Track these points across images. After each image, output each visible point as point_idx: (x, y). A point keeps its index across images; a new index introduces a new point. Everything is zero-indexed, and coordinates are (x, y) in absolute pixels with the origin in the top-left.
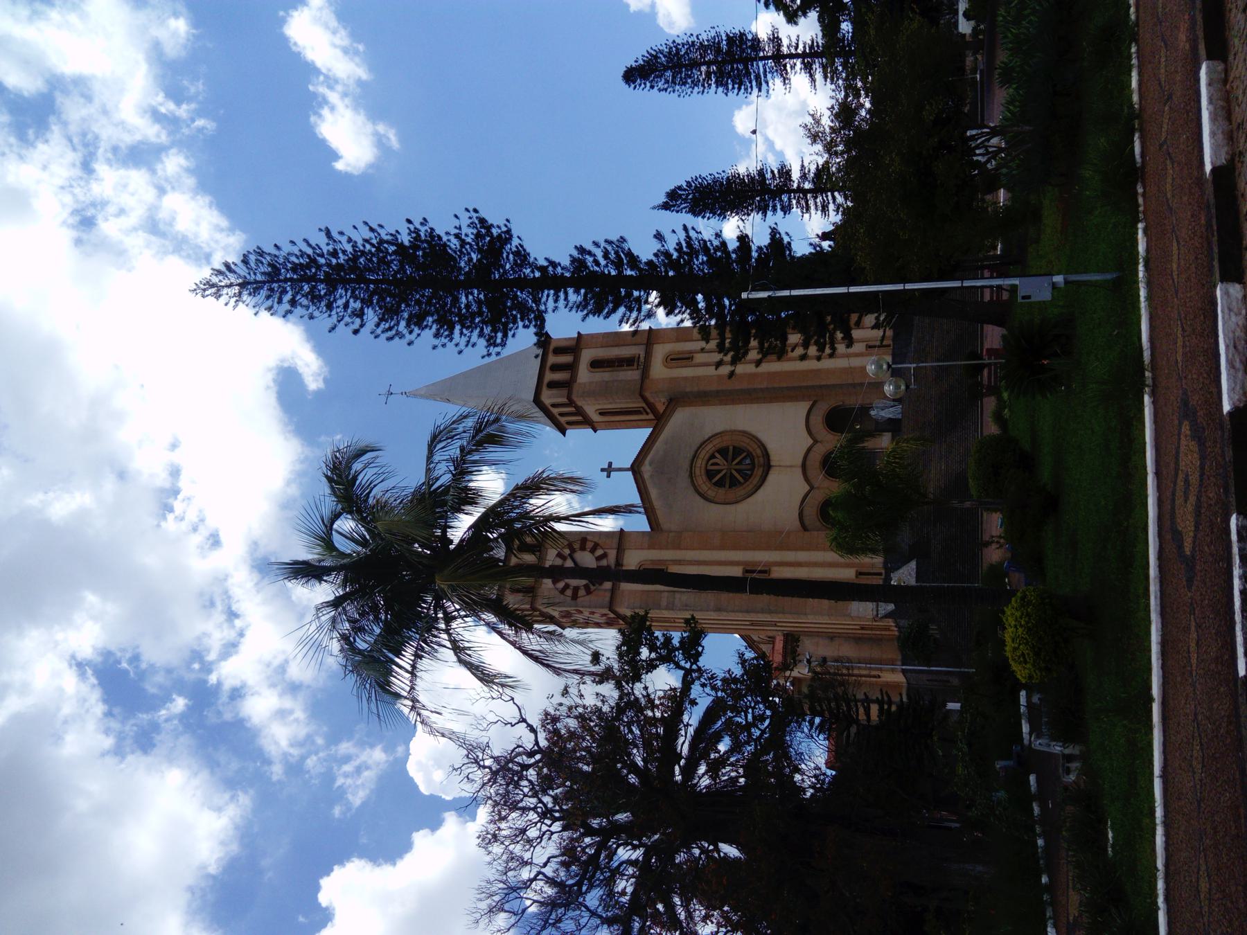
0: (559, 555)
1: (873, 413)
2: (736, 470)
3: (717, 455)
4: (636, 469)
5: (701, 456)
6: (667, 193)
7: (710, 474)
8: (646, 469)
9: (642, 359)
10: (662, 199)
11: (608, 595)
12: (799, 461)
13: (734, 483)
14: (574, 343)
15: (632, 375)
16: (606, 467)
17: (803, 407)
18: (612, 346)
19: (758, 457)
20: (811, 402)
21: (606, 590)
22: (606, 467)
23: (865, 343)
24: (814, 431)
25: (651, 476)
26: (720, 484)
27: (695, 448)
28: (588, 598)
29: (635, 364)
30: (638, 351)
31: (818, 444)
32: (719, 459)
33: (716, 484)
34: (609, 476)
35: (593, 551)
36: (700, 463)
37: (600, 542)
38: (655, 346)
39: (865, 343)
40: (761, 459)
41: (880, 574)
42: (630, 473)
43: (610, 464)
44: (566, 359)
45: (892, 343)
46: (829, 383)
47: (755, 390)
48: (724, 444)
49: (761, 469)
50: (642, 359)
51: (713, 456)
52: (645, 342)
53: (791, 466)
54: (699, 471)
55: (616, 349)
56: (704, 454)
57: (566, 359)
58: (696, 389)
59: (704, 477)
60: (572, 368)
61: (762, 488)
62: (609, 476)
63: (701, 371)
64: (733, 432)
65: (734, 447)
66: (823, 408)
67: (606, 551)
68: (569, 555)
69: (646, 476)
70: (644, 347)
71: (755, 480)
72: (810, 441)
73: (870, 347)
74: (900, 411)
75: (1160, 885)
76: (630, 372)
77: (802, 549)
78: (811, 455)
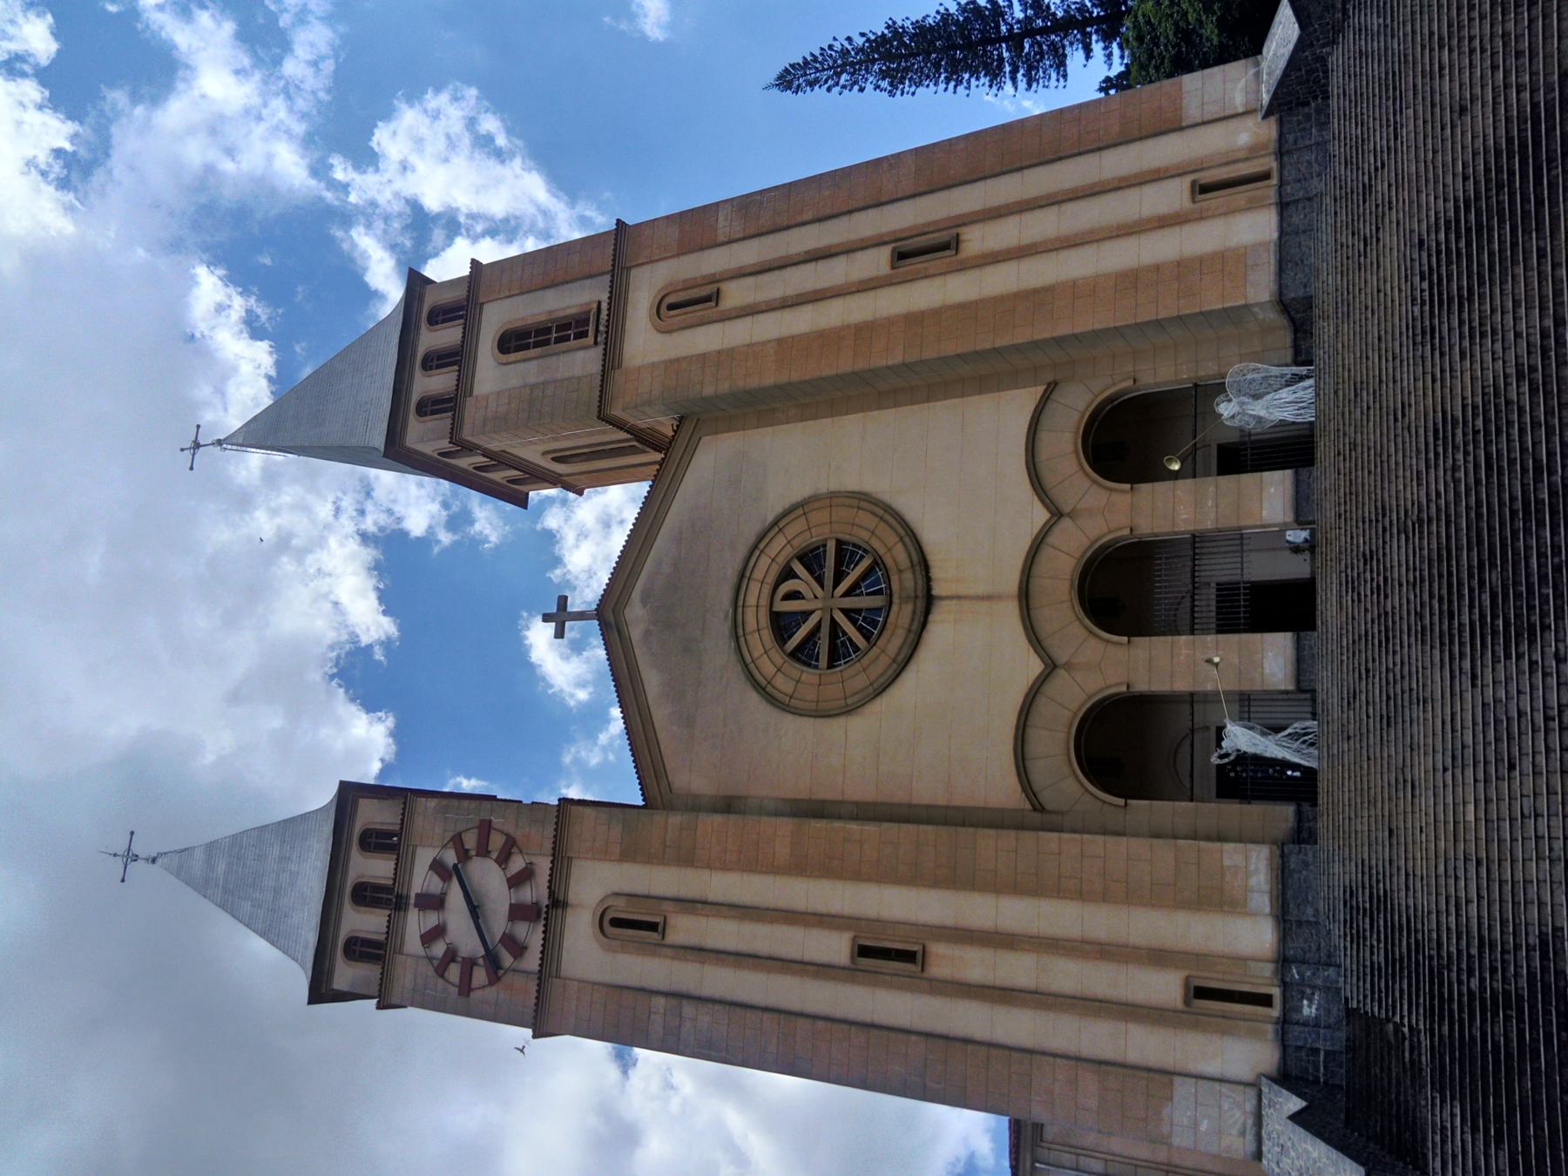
1: (1226, 409)
2: (845, 612)
3: (799, 568)
5: (758, 574)
7: (782, 625)
8: (636, 615)
12: (1010, 581)
14: (461, 293)
15: (582, 361)
17: (1017, 405)
18: (544, 288)
19: (900, 571)
20: (1041, 389)
23: (1187, 180)
24: (1049, 480)
25: (647, 634)
26: (804, 654)
27: (742, 551)
28: (491, 992)
29: (591, 333)
31: (1066, 523)
32: (803, 582)
35: (503, 860)
36: (756, 594)
37: (518, 834)
38: (634, 272)
39: (1187, 180)
40: (908, 576)
41: (1266, 1000)
44: (448, 336)
45: (1274, 165)
46: (1078, 330)
47: (875, 372)
48: (815, 537)
49: (908, 609)
51: (787, 574)
53: (988, 598)
54: (756, 620)
55: (550, 293)
56: (765, 568)
58: (725, 387)
59: (767, 635)
60: (457, 358)
61: (913, 666)
63: (738, 333)
64: (833, 498)
65: (839, 543)
66: (1076, 404)
67: (534, 859)
68: (455, 866)
69: (635, 634)
72: (1041, 515)
73: (1204, 189)
74: (1308, 395)
75: (1565, 580)
76: (580, 354)
77: (1016, 888)
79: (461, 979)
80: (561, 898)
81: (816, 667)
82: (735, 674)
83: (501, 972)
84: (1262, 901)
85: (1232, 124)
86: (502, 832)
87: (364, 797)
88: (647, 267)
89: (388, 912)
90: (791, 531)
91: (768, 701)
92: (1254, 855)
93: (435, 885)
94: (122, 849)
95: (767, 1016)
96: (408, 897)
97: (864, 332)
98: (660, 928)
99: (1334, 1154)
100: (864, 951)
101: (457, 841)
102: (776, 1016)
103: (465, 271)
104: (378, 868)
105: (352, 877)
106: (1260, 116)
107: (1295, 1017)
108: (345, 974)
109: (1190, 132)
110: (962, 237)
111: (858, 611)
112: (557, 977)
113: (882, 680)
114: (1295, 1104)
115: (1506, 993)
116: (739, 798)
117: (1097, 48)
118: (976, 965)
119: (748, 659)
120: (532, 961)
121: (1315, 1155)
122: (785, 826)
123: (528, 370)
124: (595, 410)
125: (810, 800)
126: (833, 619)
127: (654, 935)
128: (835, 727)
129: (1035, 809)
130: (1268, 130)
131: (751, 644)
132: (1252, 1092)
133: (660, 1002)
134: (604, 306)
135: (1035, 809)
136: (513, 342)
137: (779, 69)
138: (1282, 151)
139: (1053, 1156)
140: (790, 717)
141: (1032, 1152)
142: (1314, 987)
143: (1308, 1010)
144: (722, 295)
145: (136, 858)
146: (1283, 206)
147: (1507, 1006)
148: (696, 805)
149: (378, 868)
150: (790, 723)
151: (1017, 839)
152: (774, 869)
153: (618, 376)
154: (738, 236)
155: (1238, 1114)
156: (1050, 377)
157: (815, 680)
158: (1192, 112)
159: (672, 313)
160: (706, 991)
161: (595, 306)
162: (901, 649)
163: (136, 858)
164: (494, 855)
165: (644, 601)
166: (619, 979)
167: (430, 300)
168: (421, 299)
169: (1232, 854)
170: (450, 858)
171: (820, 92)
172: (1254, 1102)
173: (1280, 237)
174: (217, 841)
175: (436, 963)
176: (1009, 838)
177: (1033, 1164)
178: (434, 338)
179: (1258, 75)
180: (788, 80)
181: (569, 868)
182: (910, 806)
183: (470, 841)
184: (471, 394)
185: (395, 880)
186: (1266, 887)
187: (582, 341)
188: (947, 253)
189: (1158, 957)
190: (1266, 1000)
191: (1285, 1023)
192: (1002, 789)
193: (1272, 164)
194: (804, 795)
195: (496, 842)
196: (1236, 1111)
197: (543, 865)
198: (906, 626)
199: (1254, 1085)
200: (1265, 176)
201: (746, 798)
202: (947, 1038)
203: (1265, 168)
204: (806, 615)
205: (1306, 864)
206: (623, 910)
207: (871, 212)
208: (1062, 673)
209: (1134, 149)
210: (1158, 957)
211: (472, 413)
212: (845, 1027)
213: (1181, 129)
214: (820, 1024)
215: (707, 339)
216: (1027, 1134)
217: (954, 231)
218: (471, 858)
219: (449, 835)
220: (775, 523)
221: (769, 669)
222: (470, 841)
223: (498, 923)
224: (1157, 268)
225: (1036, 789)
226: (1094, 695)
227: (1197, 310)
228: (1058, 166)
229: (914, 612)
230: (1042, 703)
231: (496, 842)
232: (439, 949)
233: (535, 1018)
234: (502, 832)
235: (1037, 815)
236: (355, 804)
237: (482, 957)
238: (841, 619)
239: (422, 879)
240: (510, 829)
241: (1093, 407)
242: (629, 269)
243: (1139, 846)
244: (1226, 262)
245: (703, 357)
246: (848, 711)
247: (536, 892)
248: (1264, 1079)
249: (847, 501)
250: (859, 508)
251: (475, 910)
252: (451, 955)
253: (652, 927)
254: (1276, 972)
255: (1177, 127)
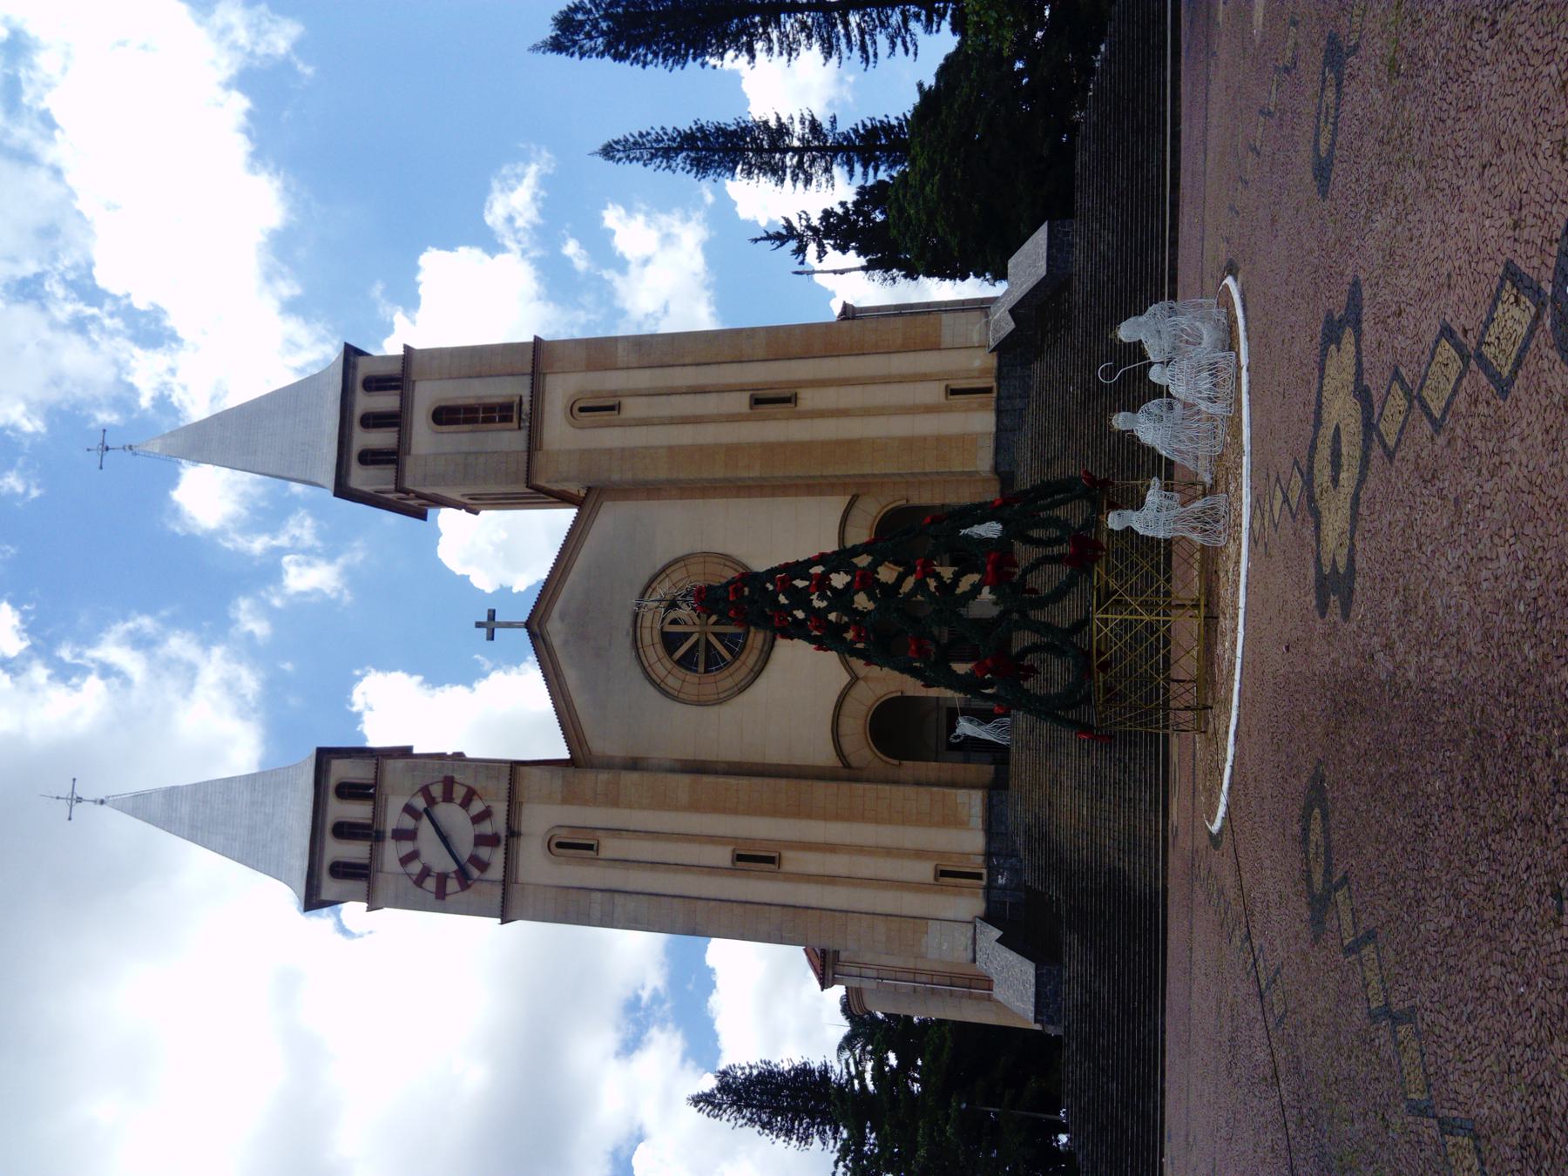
0: (409, 809)
2: (714, 634)
4: (536, 629)
6: (554, 19)
7: (670, 642)
8: (555, 628)
9: (526, 407)
10: (548, 31)
11: (498, 891)
13: (713, 663)
14: (395, 369)
15: (510, 440)
16: (484, 619)
20: (848, 498)
21: (493, 882)
22: (484, 619)
26: (687, 662)
30: (513, 389)
33: (680, 663)
34: (491, 637)
35: (465, 804)
37: (477, 787)
41: (978, 876)
42: (524, 631)
43: (492, 614)
44: (386, 402)
45: (995, 384)
50: (526, 407)
52: (529, 370)
54: (650, 637)
57: (386, 402)
58: (629, 476)
59: (659, 648)
60: (393, 420)
61: (764, 674)
62: (491, 637)
68: (426, 810)
70: (527, 380)
71: (750, 658)
76: (507, 435)
77: (838, 817)
78: (844, 729)
79: (437, 887)
80: (516, 829)
81: (696, 671)
82: (636, 672)
83: (469, 882)
84: (977, 821)
85: (970, 352)
86: (463, 785)
87: (334, 758)
88: (561, 376)
89: (369, 843)
90: (676, 576)
91: (661, 693)
92: (974, 796)
93: (408, 822)
94: (66, 792)
95: (676, 901)
96: (384, 832)
97: (732, 450)
98: (595, 848)
99: (1021, 958)
100: (740, 858)
101: (425, 791)
102: (681, 900)
103: (400, 351)
104: (357, 811)
105: (330, 820)
106: (987, 351)
107: (994, 884)
108: (329, 887)
109: (943, 352)
110: (799, 396)
111: (725, 635)
112: (516, 883)
113: (743, 683)
114: (997, 933)
115: (1096, 889)
116: (643, 758)
117: (858, 169)
118: (813, 863)
119: (646, 665)
120: (496, 872)
121: (1011, 959)
122: (686, 779)
123: (459, 439)
124: (523, 475)
125: (695, 761)
126: (707, 639)
127: (591, 853)
128: (712, 712)
129: (845, 767)
130: (992, 361)
131: (648, 654)
132: (971, 927)
133: (598, 895)
134: (526, 400)
135: (845, 767)
136: (444, 416)
137: (604, 141)
138: (1000, 376)
139: (846, 970)
140: (678, 706)
141: (833, 968)
142: (1003, 868)
143: (1001, 881)
144: (622, 406)
145: (79, 800)
146: (999, 412)
147: (1096, 895)
148: (609, 765)
149: (357, 811)
150: (678, 708)
151: (838, 788)
152: (676, 808)
153: (540, 458)
154: (633, 365)
155: (963, 938)
156: (854, 491)
157: (696, 680)
158: (947, 340)
159: (583, 414)
160: (630, 888)
161: (517, 399)
162: (756, 662)
163: (79, 800)
164: (458, 801)
165: (562, 617)
166: (566, 883)
167: (363, 369)
168: (355, 367)
169: (961, 795)
170: (420, 803)
171: (638, 165)
172: (972, 931)
173: (997, 432)
174: (178, 787)
175: (414, 878)
176: (833, 786)
177: (833, 975)
178: (367, 402)
179: (987, 323)
180: (608, 151)
181: (520, 809)
182: (764, 764)
183: (437, 791)
184: (409, 454)
185: (373, 820)
186: (980, 814)
187: (508, 425)
188: (789, 405)
189: (920, 854)
190: (978, 876)
191: (989, 889)
192: (824, 755)
193: (991, 382)
194: (690, 757)
195: (459, 793)
196: (963, 936)
197: (500, 809)
198: (760, 647)
199: (972, 923)
200: (988, 390)
201: (648, 758)
202: (795, 907)
203: (990, 385)
204: (687, 635)
205: (1002, 802)
206: (564, 836)
207: (734, 365)
208: (861, 684)
209: (911, 356)
210: (920, 854)
211: (410, 465)
212: (729, 904)
213: (940, 349)
214: (712, 903)
215: (609, 438)
216: (830, 958)
217: (793, 391)
218: (437, 803)
219: (417, 788)
220: (663, 570)
221: (662, 672)
222: (437, 791)
223: (465, 849)
224: (924, 439)
225: (846, 754)
226: (882, 697)
227: (947, 470)
228: (862, 358)
229: (765, 640)
230: (849, 700)
231: (459, 793)
232: (415, 867)
233: (502, 911)
234: (463, 785)
235: (847, 770)
236: (328, 763)
237: (455, 872)
238: (712, 639)
239: (394, 818)
240: (470, 783)
241: (882, 514)
242: (545, 374)
243: (910, 791)
244: (964, 442)
245: (610, 451)
246: (720, 702)
247: (498, 824)
248: (978, 920)
249: (716, 560)
250: (725, 565)
251: (445, 839)
252: (426, 872)
253: (589, 847)
254: (984, 861)
255: (936, 347)
